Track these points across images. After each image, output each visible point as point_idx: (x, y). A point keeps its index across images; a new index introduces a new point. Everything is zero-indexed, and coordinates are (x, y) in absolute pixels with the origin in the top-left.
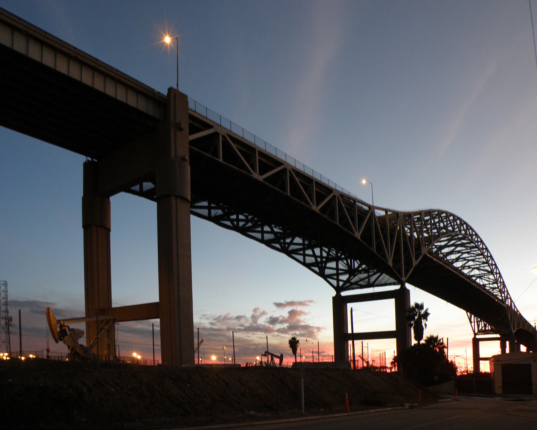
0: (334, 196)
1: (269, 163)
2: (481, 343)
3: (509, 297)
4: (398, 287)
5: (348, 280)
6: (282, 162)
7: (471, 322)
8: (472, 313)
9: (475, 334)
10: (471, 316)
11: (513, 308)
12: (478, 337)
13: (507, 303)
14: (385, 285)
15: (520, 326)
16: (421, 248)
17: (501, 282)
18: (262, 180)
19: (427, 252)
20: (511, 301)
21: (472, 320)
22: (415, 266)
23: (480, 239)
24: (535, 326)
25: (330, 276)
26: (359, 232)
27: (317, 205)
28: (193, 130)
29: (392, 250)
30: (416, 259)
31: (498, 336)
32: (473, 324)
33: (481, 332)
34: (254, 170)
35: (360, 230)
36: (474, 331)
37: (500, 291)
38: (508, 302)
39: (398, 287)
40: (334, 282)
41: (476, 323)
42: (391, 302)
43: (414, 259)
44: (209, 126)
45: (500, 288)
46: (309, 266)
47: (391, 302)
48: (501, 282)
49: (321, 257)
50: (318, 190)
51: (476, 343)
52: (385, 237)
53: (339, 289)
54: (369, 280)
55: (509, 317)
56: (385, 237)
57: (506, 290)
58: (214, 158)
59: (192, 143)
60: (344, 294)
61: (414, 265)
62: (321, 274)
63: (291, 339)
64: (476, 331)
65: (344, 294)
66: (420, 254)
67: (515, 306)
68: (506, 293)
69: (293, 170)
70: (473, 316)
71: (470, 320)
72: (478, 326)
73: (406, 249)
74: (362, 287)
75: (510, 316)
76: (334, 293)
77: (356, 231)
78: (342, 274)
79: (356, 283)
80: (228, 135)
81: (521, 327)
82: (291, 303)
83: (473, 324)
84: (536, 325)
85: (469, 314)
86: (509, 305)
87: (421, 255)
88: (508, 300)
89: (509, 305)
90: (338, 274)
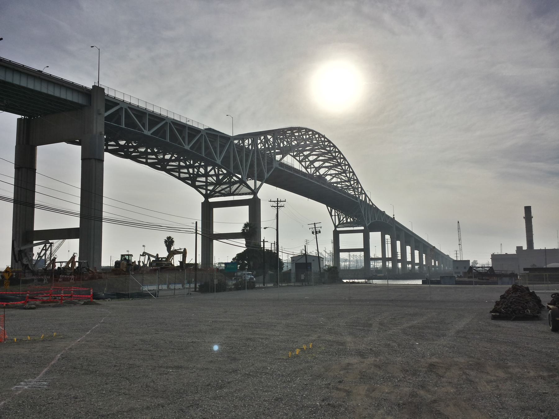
0: (202, 135)
1: (156, 119)
2: (341, 235)
3: (363, 192)
4: (251, 197)
5: (213, 190)
6: (164, 118)
7: (331, 216)
8: (332, 208)
9: (336, 227)
10: (331, 211)
11: (368, 202)
12: (338, 229)
13: (361, 198)
14: (243, 194)
15: (375, 219)
16: (273, 162)
17: (354, 180)
18: (150, 135)
19: (278, 165)
20: (366, 196)
21: (333, 214)
22: (267, 178)
23: (332, 144)
24: (394, 217)
25: (200, 187)
26: (220, 160)
27: (188, 144)
28: (107, 109)
29: (247, 170)
30: (268, 173)
31: (362, 228)
32: (333, 217)
33: (341, 224)
34: (145, 129)
35: (221, 158)
36: (335, 224)
37: (354, 189)
38: (362, 198)
39: (251, 197)
40: (204, 192)
41: (337, 217)
42: (247, 208)
43: (266, 173)
44: (117, 104)
45: (353, 186)
46: (184, 180)
47: (247, 208)
48: (354, 180)
49: (193, 174)
50: (189, 132)
51: (336, 234)
52: (241, 161)
53: (207, 196)
54: (230, 189)
55: (363, 212)
56: (241, 161)
57: (360, 186)
58: (119, 126)
59: (107, 118)
60: (211, 200)
61: (266, 177)
62: (193, 185)
63: (166, 239)
64: (337, 223)
65: (211, 200)
66: (272, 168)
67: (370, 200)
68: (360, 189)
69: (172, 122)
70: (333, 211)
71: (331, 213)
72: (339, 219)
73: (259, 164)
74: (224, 195)
75: (363, 211)
76: (203, 199)
77: (218, 159)
78: (209, 185)
79: (219, 192)
80: (128, 107)
81: (377, 220)
82: (169, 228)
83: (333, 217)
84: (394, 216)
85: (329, 208)
86: (363, 200)
87: (273, 168)
88: (362, 196)
89: (363, 200)
90: (207, 186)
